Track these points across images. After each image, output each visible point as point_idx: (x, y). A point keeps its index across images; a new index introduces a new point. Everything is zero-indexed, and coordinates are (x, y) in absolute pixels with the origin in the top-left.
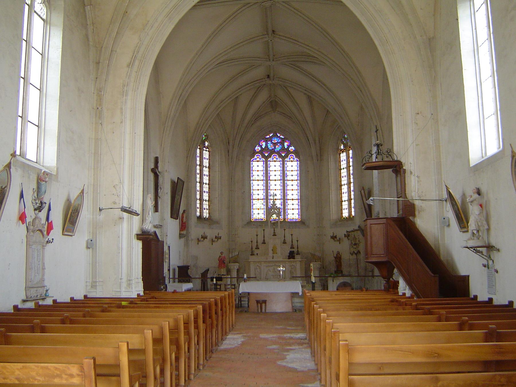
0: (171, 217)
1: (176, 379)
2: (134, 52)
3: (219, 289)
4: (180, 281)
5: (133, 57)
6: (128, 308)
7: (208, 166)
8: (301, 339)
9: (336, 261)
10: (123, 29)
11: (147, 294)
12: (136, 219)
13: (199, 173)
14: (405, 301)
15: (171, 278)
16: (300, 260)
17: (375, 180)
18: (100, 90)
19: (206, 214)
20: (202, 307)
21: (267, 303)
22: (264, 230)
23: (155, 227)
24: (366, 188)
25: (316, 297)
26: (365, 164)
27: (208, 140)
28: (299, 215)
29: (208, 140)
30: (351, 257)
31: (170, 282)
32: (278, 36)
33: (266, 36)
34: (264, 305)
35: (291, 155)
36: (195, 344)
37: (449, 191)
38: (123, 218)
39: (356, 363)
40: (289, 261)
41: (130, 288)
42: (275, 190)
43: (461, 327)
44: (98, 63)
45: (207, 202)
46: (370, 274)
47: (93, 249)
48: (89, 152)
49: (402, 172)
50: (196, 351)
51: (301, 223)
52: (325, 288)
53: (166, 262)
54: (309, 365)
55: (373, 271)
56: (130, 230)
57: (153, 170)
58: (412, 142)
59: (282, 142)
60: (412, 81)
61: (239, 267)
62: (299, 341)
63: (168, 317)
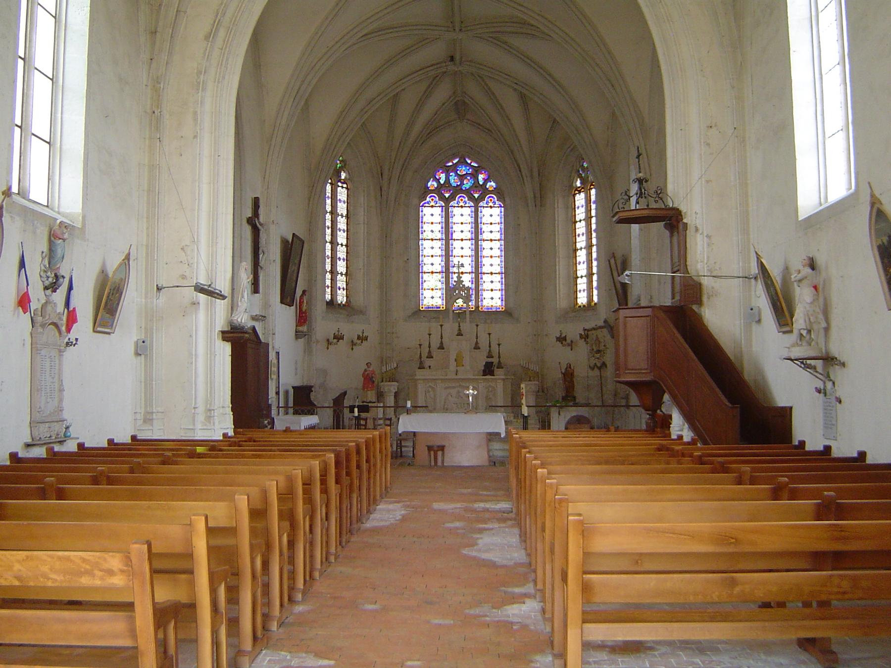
0: (282, 302)
3: (363, 425)
4: (296, 413)
5: (215, 22)
7: (345, 213)
9: (565, 380)
11: (239, 433)
12: (221, 306)
16: (503, 377)
17: (635, 242)
18: (157, 80)
19: (341, 297)
20: (335, 457)
22: (441, 326)
23: (254, 318)
24: (619, 255)
26: (617, 213)
27: (345, 170)
28: (502, 300)
30: (591, 373)
34: (440, 453)
36: (322, 520)
37: (762, 262)
38: (198, 303)
41: (210, 423)
42: (462, 256)
43: (776, 494)
44: (154, 33)
45: (344, 276)
46: (623, 402)
47: (146, 356)
48: (139, 188)
51: (506, 314)
52: (545, 425)
53: (272, 379)
54: (516, 555)
55: (627, 398)
57: (250, 221)
58: (700, 176)
61: (398, 389)
63: (276, 473)
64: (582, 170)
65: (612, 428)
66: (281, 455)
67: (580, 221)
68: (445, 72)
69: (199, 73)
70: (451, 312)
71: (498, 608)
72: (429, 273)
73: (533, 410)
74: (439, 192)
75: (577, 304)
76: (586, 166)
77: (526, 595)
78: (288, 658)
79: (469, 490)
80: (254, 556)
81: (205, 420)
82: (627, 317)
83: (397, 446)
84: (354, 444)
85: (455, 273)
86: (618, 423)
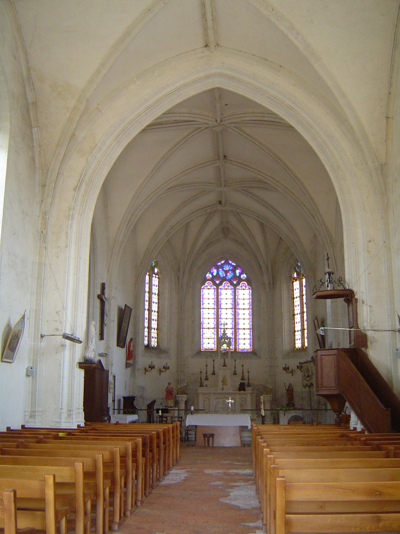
0: (118, 346)
4: (125, 413)
5: (80, 180)
7: (157, 293)
8: (248, 476)
9: (288, 394)
10: (71, 151)
15: (116, 409)
17: (329, 310)
18: (45, 213)
19: (154, 343)
20: (142, 441)
21: (215, 438)
22: (214, 360)
23: (100, 355)
24: (320, 318)
25: (263, 431)
27: (157, 267)
28: (251, 345)
30: (304, 389)
31: (114, 413)
34: (211, 439)
36: (132, 479)
38: (65, 345)
39: (294, 502)
40: (238, 393)
41: (70, 418)
44: (44, 186)
46: (324, 407)
47: (33, 377)
48: (32, 276)
49: (354, 301)
51: (253, 354)
52: (276, 421)
53: (110, 392)
54: (253, 502)
55: (326, 405)
58: (364, 270)
61: (187, 398)
62: (245, 477)
63: (105, 449)
64: (297, 267)
68: (216, 210)
70: (219, 352)
73: (269, 412)
75: (295, 347)
77: (257, 528)
79: (228, 462)
81: (67, 417)
82: (323, 355)
84: (155, 432)
85: (222, 329)
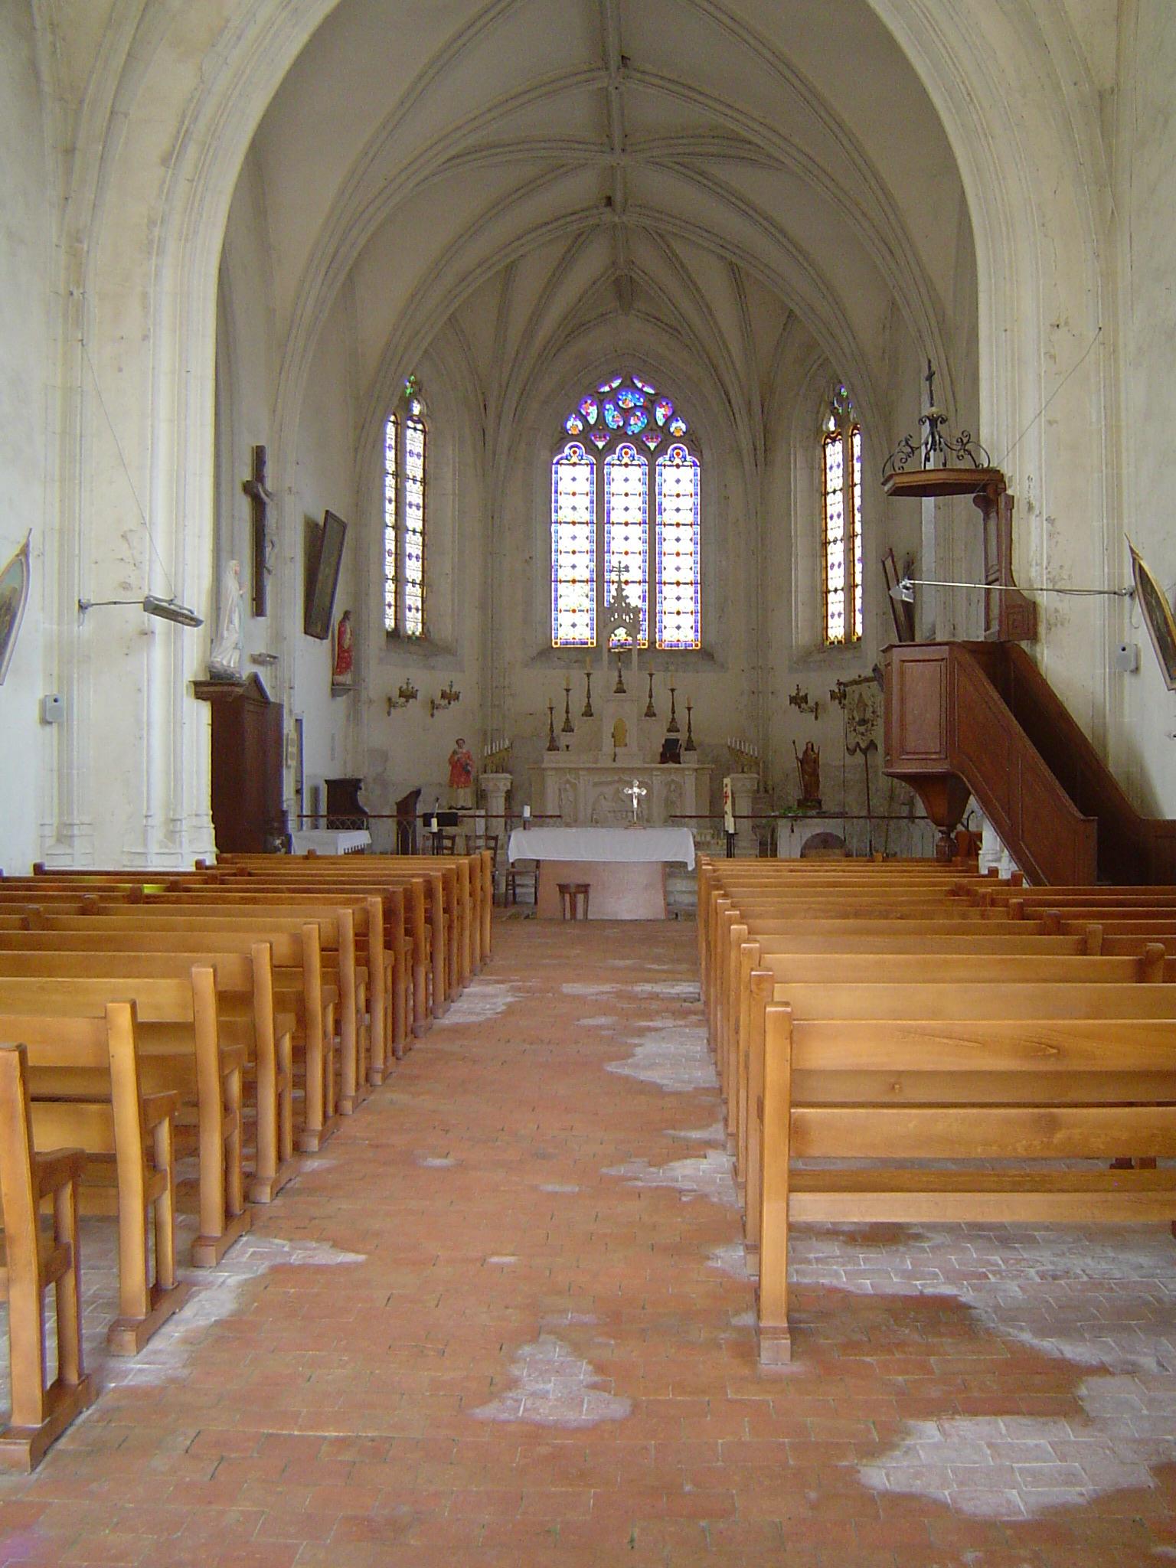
0: (306, 633)
1: (295, 1113)
2: (184, 116)
3: (446, 848)
4: (331, 826)
6: (162, 903)
7: (419, 475)
11: (226, 861)
12: (192, 636)
13: (393, 498)
14: (992, 894)
16: (697, 766)
17: (928, 529)
19: (413, 624)
20: (384, 903)
22: (588, 675)
23: (256, 660)
24: (900, 553)
26: (891, 477)
29: (419, 398)
30: (849, 760)
32: (639, 75)
33: (602, 73)
34: (580, 897)
35: (676, 448)
36: (357, 1011)
37: (1140, 567)
41: (174, 842)
42: (626, 553)
43: (1142, 971)
44: (70, 151)
45: (418, 586)
47: (60, 725)
49: (1002, 505)
50: (363, 1030)
51: (704, 654)
52: (767, 849)
53: (288, 767)
55: (911, 804)
56: (175, 667)
57: (249, 489)
59: (650, 406)
60: (1043, 225)
62: (678, 1005)
63: (276, 929)
65: (879, 856)
66: (292, 897)
67: (834, 492)
69: (152, 223)
70: (605, 651)
71: (659, 1165)
72: (568, 581)
74: (586, 438)
76: (845, 394)
77: (710, 1144)
78: (286, 1249)
79: (629, 962)
80: (226, 1072)
81: (165, 838)
83: (507, 885)
86: (894, 848)
